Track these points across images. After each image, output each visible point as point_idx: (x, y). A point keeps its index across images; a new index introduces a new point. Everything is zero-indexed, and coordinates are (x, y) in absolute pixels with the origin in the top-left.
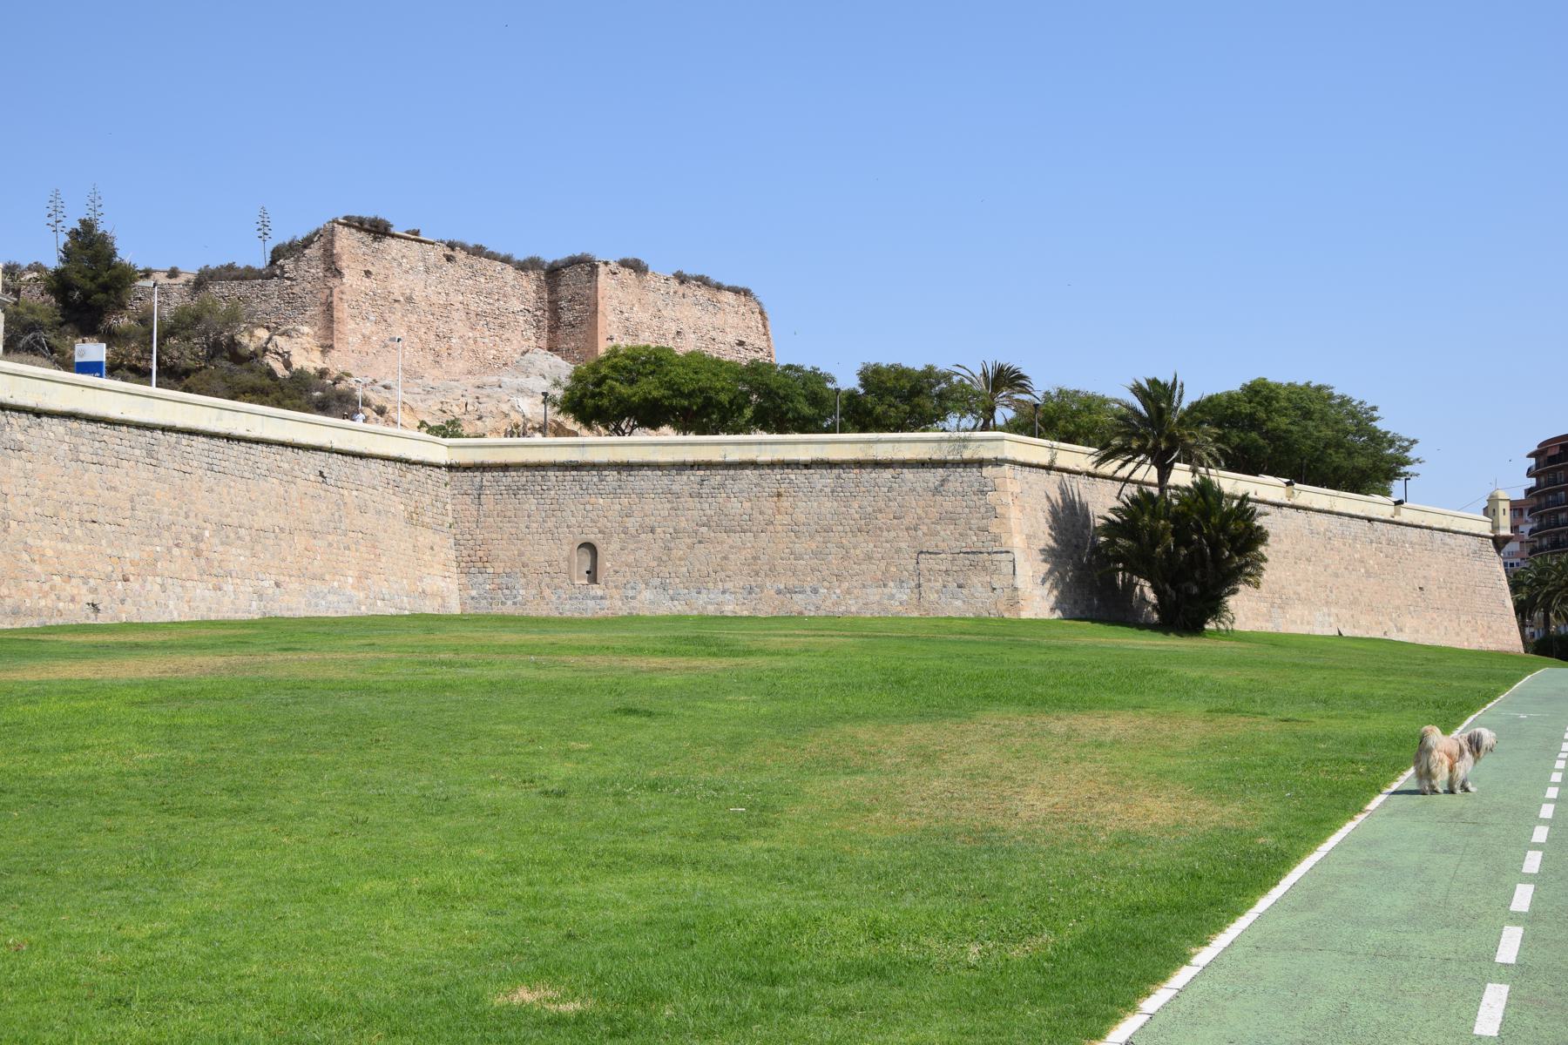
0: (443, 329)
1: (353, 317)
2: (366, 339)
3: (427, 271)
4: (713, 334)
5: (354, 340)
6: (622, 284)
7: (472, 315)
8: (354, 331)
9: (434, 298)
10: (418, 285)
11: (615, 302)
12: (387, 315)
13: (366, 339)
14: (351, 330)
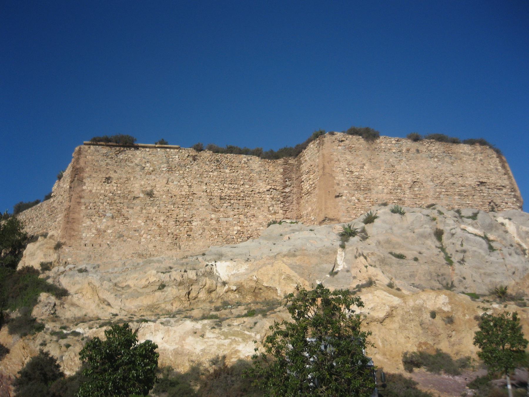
0: (183, 214)
1: (89, 216)
2: (100, 233)
3: (170, 170)
4: (453, 179)
5: (88, 235)
6: (350, 149)
7: (217, 201)
8: (89, 228)
9: (175, 191)
11: (343, 165)
12: (124, 211)
13: (100, 233)
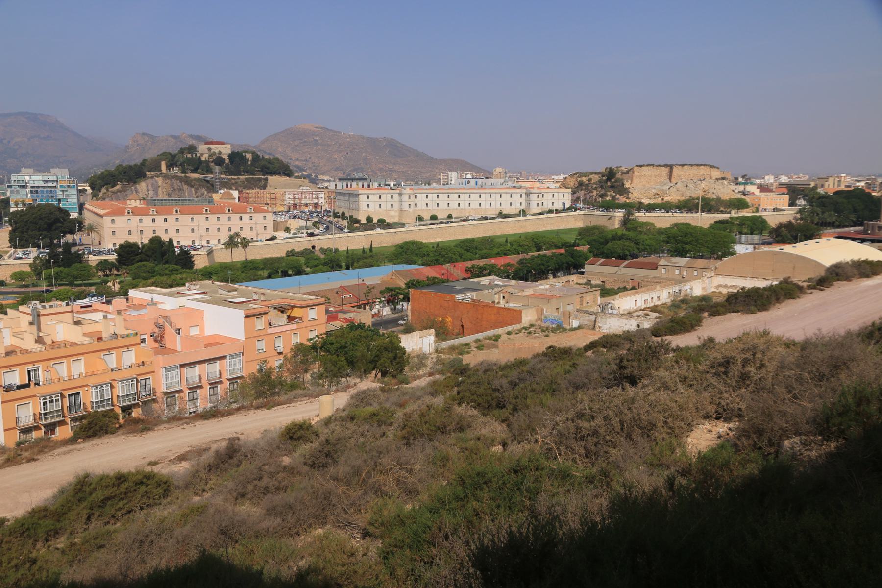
10: (646, 173)
14: (635, 181)
